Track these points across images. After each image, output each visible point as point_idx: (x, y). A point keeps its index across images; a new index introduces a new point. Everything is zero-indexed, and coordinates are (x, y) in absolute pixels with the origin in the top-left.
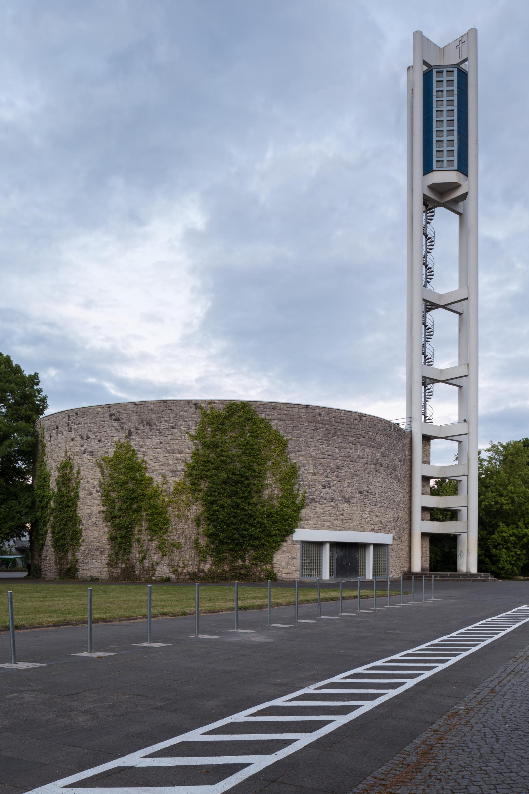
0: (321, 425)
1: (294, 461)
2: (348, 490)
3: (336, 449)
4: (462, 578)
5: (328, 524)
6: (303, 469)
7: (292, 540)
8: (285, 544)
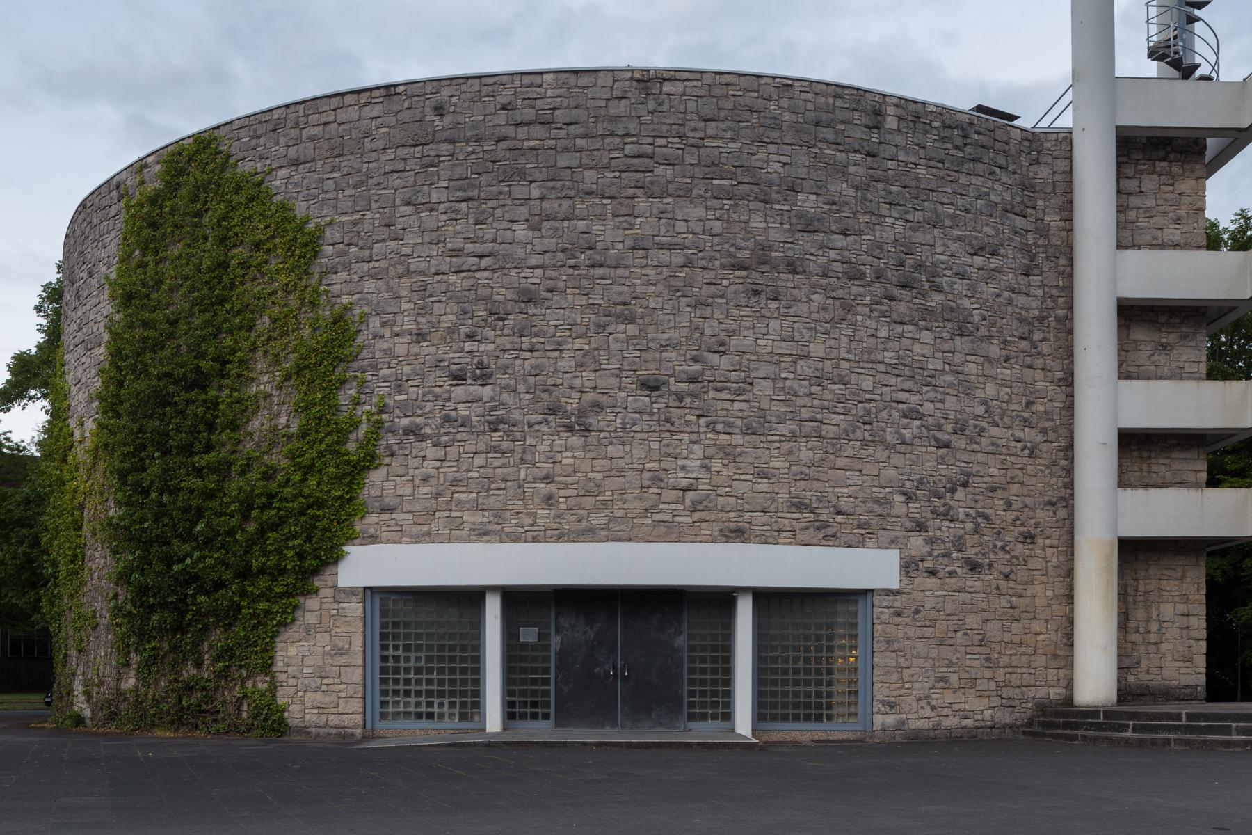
0: (445, 148)
1: (345, 299)
2: (578, 382)
3: (515, 226)
4: (1240, 731)
5: (478, 518)
6: (375, 323)
7: (335, 587)
8: (312, 603)
